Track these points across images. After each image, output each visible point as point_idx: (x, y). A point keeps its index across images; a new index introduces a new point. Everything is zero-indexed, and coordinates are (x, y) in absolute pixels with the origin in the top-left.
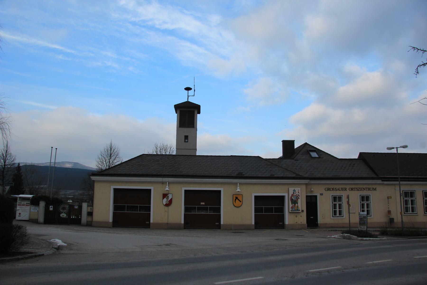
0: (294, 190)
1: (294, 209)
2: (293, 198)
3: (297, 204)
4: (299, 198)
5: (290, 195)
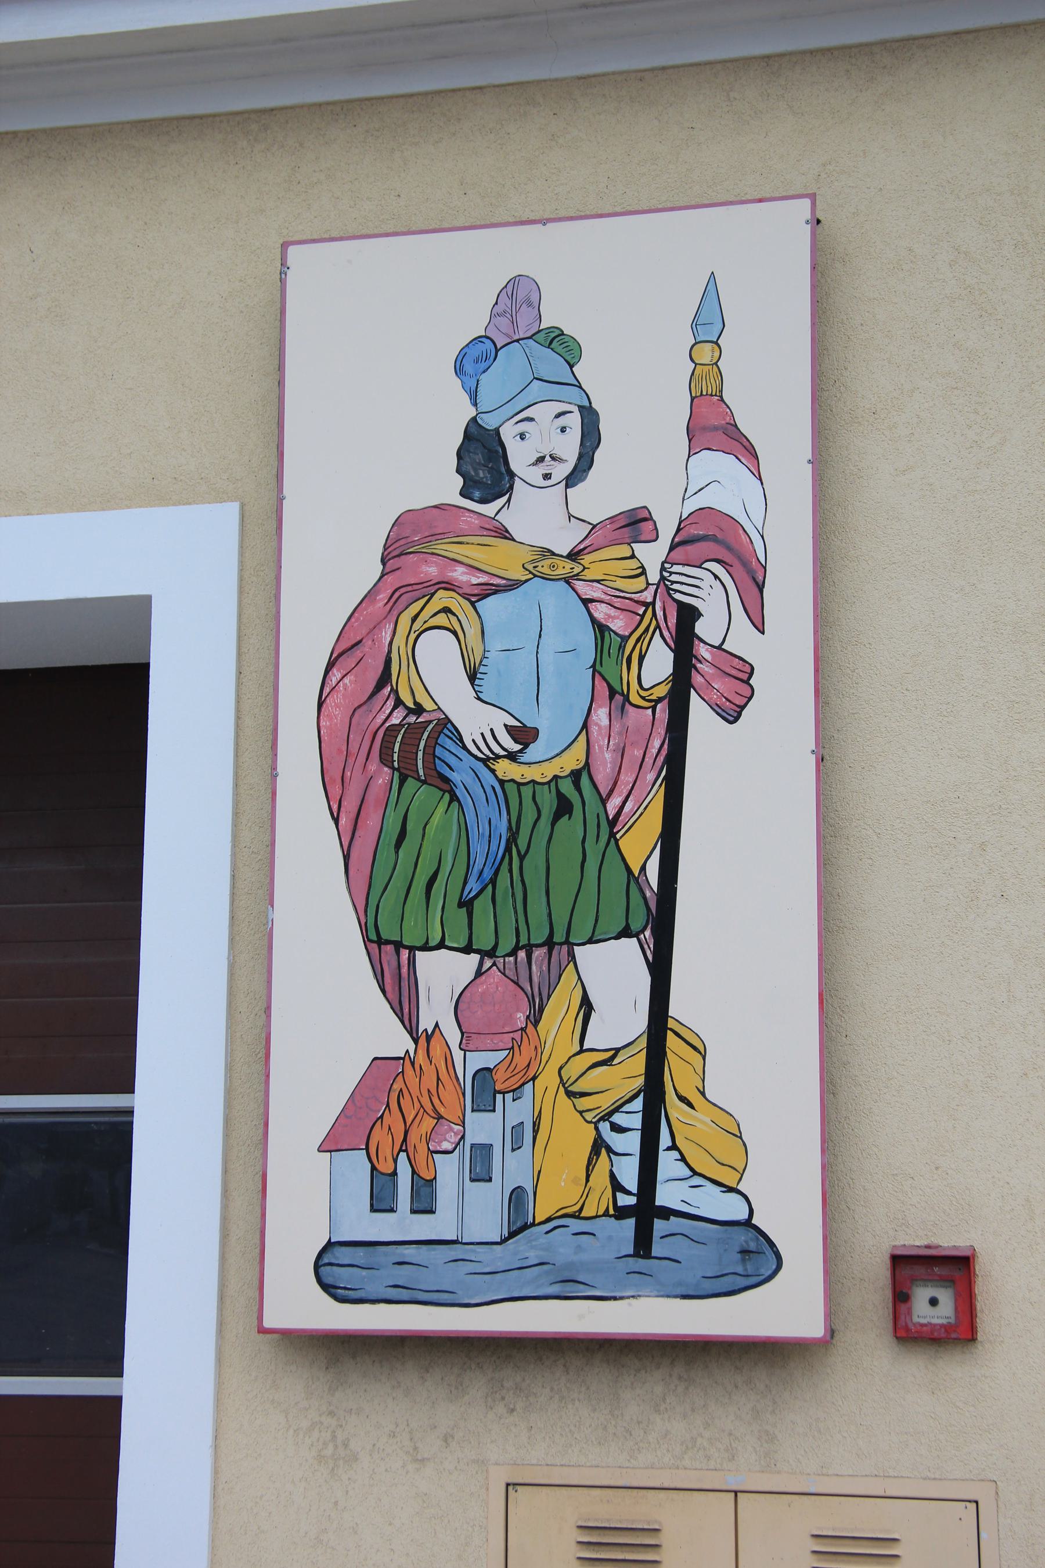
0: (522, 340)
1: (467, 1210)
2: (437, 671)
3: (613, 970)
4: (697, 678)
5: (331, 575)
